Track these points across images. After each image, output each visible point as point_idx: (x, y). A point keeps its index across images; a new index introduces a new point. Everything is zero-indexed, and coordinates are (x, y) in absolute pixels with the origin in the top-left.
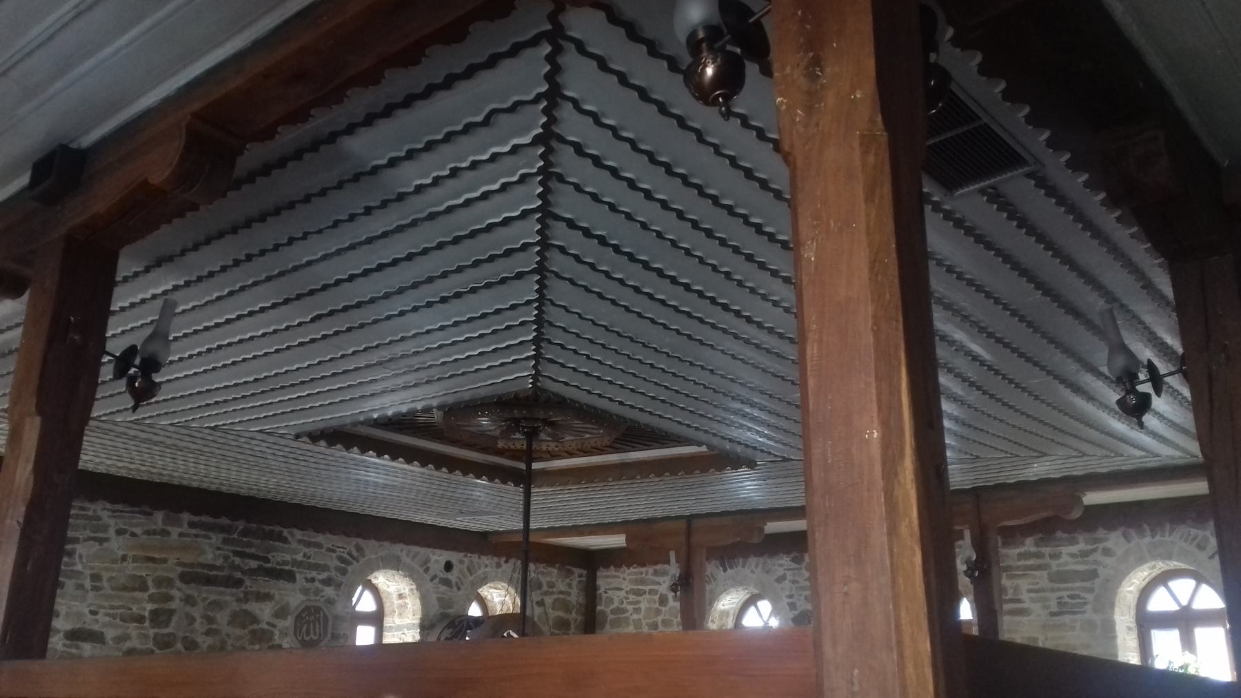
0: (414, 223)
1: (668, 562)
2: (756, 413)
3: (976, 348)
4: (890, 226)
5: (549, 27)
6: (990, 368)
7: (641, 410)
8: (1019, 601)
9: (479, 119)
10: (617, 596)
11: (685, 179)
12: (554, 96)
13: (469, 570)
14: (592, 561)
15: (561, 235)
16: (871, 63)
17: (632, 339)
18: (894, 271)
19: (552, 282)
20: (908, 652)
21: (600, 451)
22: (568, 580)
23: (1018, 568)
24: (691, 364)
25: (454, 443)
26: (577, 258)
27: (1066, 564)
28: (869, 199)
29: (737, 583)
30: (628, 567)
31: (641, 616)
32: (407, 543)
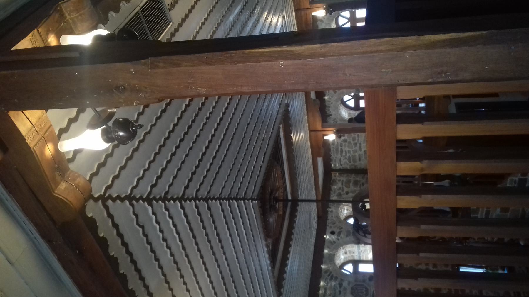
2: (266, 104)
3: (236, 11)
6: (245, 5)
7: (265, 153)
9: (141, 230)
14: (328, 170)
18: (210, 55)
20: (374, 49)
22: (337, 181)
25: (280, 233)
28: (179, 65)
29: (337, 109)
30: (330, 156)
31: (351, 150)
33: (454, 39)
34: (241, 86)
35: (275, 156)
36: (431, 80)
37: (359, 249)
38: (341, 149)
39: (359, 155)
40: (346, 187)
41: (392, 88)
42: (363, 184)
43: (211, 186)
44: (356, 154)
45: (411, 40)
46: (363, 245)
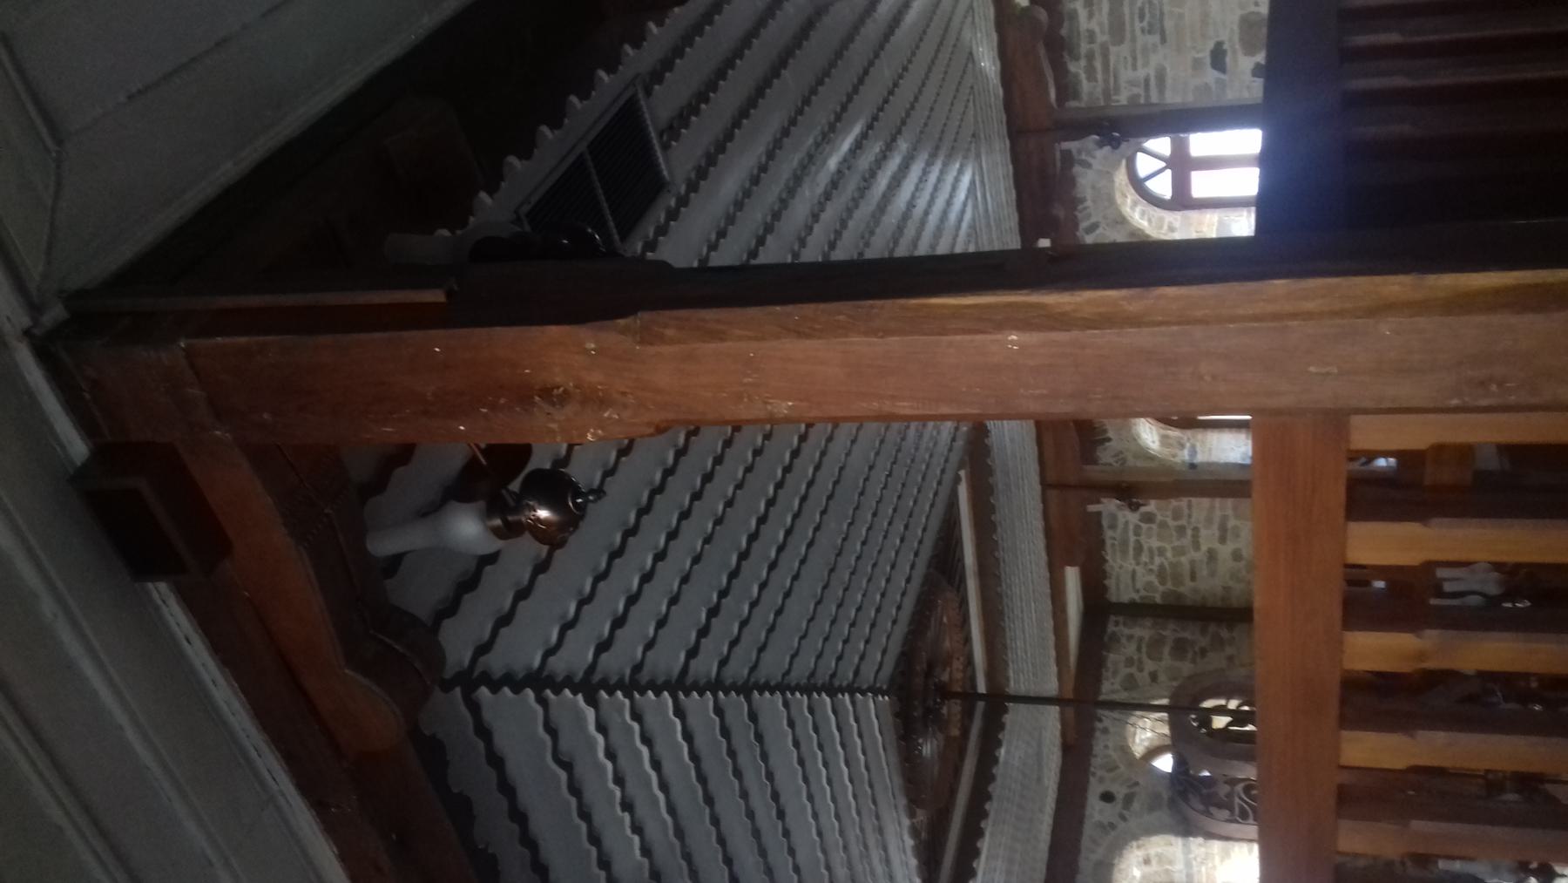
0: (687, 857)
1: (1099, 514)
3: (846, 145)
4: (754, 312)
5: (458, 690)
6: (870, 127)
8: (1147, 81)
10: (1143, 578)
11: (643, 511)
12: (540, 681)
13: (1111, 770)
14: (1098, 607)
15: (706, 666)
16: (553, 330)
17: (832, 570)
18: (809, 309)
19: (762, 675)
21: (964, 602)
22: (1124, 640)
23: (1106, 81)
24: (862, 494)
25: (953, 792)
26: (734, 643)
27: (1101, 24)
28: (719, 336)
32: (1079, 851)
33: (1529, 286)
34: (893, 397)
35: (944, 563)
36: (1455, 402)
37: (1187, 851)
38: (1138, 542)
39: (1192, 562)
40: (1150, 657)
41: (1336, 420)
42: (1203, 652)
43: (762, 649)
44: (1184, 559)
45: (1396, 286)
46: (1200, 840)
